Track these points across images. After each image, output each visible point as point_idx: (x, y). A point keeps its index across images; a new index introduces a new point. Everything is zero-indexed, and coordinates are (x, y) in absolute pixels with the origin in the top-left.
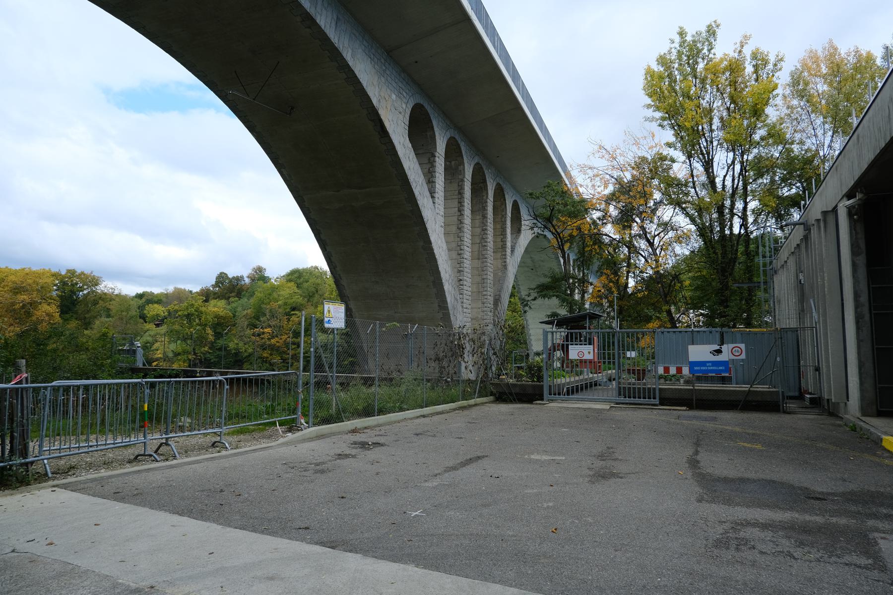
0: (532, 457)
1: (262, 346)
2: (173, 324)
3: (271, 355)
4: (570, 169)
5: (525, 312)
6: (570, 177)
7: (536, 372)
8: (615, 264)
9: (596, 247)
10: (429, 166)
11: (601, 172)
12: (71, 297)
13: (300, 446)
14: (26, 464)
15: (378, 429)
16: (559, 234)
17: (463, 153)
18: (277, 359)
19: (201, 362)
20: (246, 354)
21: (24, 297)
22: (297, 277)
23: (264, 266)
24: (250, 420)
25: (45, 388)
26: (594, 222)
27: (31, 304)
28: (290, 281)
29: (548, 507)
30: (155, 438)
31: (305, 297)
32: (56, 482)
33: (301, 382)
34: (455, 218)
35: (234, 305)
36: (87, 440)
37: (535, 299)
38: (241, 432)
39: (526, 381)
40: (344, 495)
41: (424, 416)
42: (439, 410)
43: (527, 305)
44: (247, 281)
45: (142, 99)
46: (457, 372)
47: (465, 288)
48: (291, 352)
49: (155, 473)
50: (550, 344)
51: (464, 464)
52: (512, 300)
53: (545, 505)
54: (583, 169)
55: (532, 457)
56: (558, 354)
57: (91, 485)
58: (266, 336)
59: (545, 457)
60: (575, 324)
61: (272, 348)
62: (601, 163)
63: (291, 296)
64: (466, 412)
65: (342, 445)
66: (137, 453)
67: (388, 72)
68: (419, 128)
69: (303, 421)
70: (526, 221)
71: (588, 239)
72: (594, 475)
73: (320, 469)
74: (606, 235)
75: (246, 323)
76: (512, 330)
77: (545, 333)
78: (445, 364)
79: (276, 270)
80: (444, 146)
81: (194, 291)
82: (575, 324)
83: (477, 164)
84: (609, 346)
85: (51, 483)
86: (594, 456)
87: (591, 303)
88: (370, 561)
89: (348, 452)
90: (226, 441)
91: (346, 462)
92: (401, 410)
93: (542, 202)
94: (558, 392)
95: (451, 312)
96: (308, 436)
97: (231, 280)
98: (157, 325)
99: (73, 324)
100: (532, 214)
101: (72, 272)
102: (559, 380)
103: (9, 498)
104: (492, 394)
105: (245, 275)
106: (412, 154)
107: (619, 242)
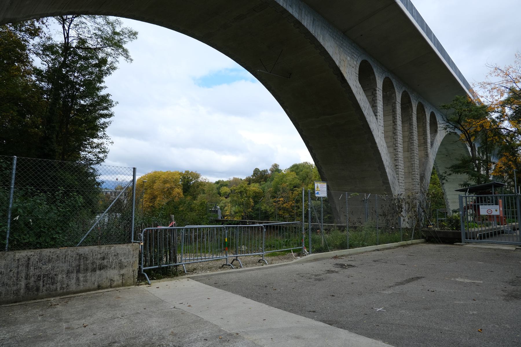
0: (457, 279)
1: (279, 208)
2: (234, 196)
3: (284, 213)
4: (472, 86)
5: (443, 184)
6: (473, 92)
7: (455, 223)
8: (512, 148)
9: (496, 137)
10: (372, 96)
11: (497, 86)
12: (187, 184)
13: (305, 264)
14: (176, 266)
15: (349, 256)
16: (466, 131)
17: (395, 86)
18: (287, 215)
19: (248, 217)
20: (271, 213)
21: (168, 185)
22: (296, 168)
23: (278, 164)
24: (277, 249)
25: (182, 229)
26: (493, 121)
27: (171, 188)
28: (292, 171)
29: (473, 314)
30: (231, 256)
31: (301, 180)
32: (189, 276)
33: (304, 228)
34: (391, 127)
35: (263, 186)
36: (201, 256)
37: (450, 175)
38: (272, 255)
39: (447, 229)
40: (333, 294)
41: (378, 250)
42: (387, 247)
43: (444, 179)
44: (269, 172)
45: (210, 81)
46: (398, 223)
47: (400, 170)
48: (295, 211)
49: (232, 275)
50: (464, 205)
51: (412, 280)
52: (433, 177)
53: (471, 313)
54: (483, 85)
55: (457, 279)
56: (470, 211)
57: (204, 278)
58: (281, 202)
59: (469, 281)
60: (483, 191)
61: (284, 209)
62: (497, 80)
63: (293, 179)
64: (406, 249)
65: (329, 265)
66: (223, 264)
67: (344, 45)
68: (365, 76)
69: (306, 250)
70: (441, 124)
71: (489, 132)
72: (508, 296)
73: (318, 279)
74: (504, 128)
75: (270, 195)
76: (435, 196)
77: (461, 198)
78: (389, 218)
79: (284, 166)
80: (382, 83)
81: (243, 179)
82: (483, 191)
83: (404, 92)
84: (512, 205)
85: (186, 276)
86: (506, 282)
87: (494, 176)
88: (353, 335)
89: (333, 270)
90: (266, 259)
91: (332, 275)
92: (363, 246)
93: (453, 110)
94: (472, 237)
95: (391, 186)
96: (309, 259)
97: (261, 172)
98: (226, 198)
99: (189, 198)
100: (445, 119)
101: (187, 172)
102: (473, 229)
103: (170, 282)
104: (423, 237)
105: (268, 169)
106: (362, 91)
107: (515, 132)
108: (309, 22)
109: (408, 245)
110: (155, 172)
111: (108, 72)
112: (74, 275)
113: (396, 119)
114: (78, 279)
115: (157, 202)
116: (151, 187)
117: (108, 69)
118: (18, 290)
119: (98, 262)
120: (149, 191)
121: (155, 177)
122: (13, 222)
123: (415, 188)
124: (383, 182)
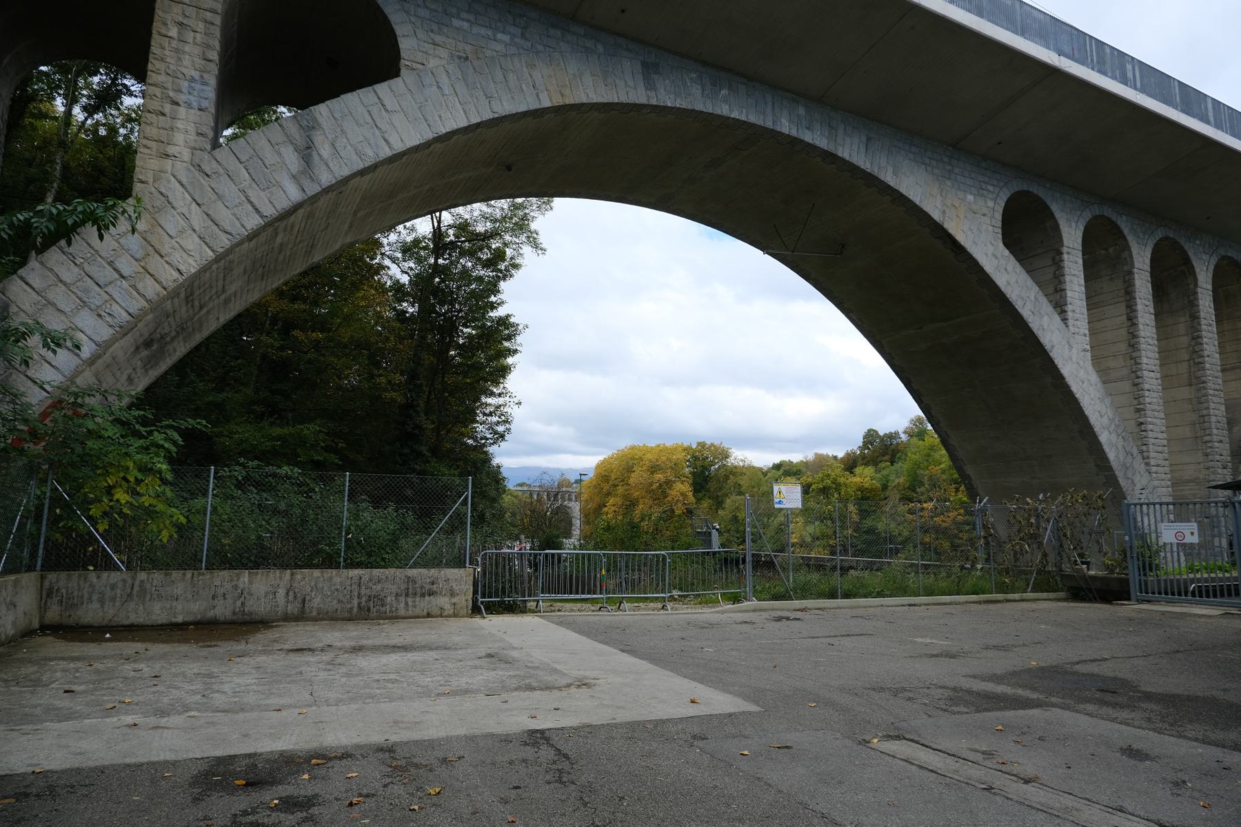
12: (703, 472)
17: (1126, 232)
21: (659, 476)
34: (1123, 332)
35: (885, 472)
44: (904, 437)
49: (610, 617)
58: (925, 513)
61: (938, 530)
75: (898, 497)
97: (882, 439)
101: (702, 445)
105: (901, 430)
106: (1012, 263)
108: (855, 147)
109: (1008, 601)
110: (632, 448)
111: (506, 275)
112: (402, 599)
113: (1136, 311)
114: (406, 603)
115: (637, 512)
116: (624, 481)
117: (507, 270)
118: (352, 608)
119: (427, 587)
120: (620, 490)
121: (633, 459)
122: (347, 540)
123: (1212, 477)
124: (1097, 466)
